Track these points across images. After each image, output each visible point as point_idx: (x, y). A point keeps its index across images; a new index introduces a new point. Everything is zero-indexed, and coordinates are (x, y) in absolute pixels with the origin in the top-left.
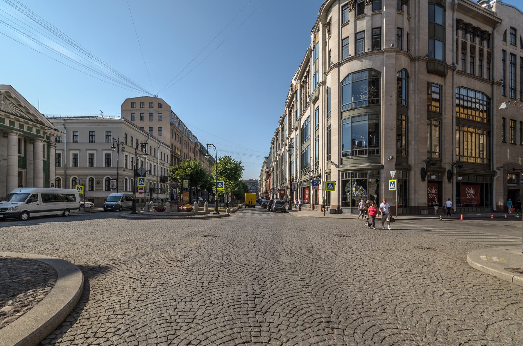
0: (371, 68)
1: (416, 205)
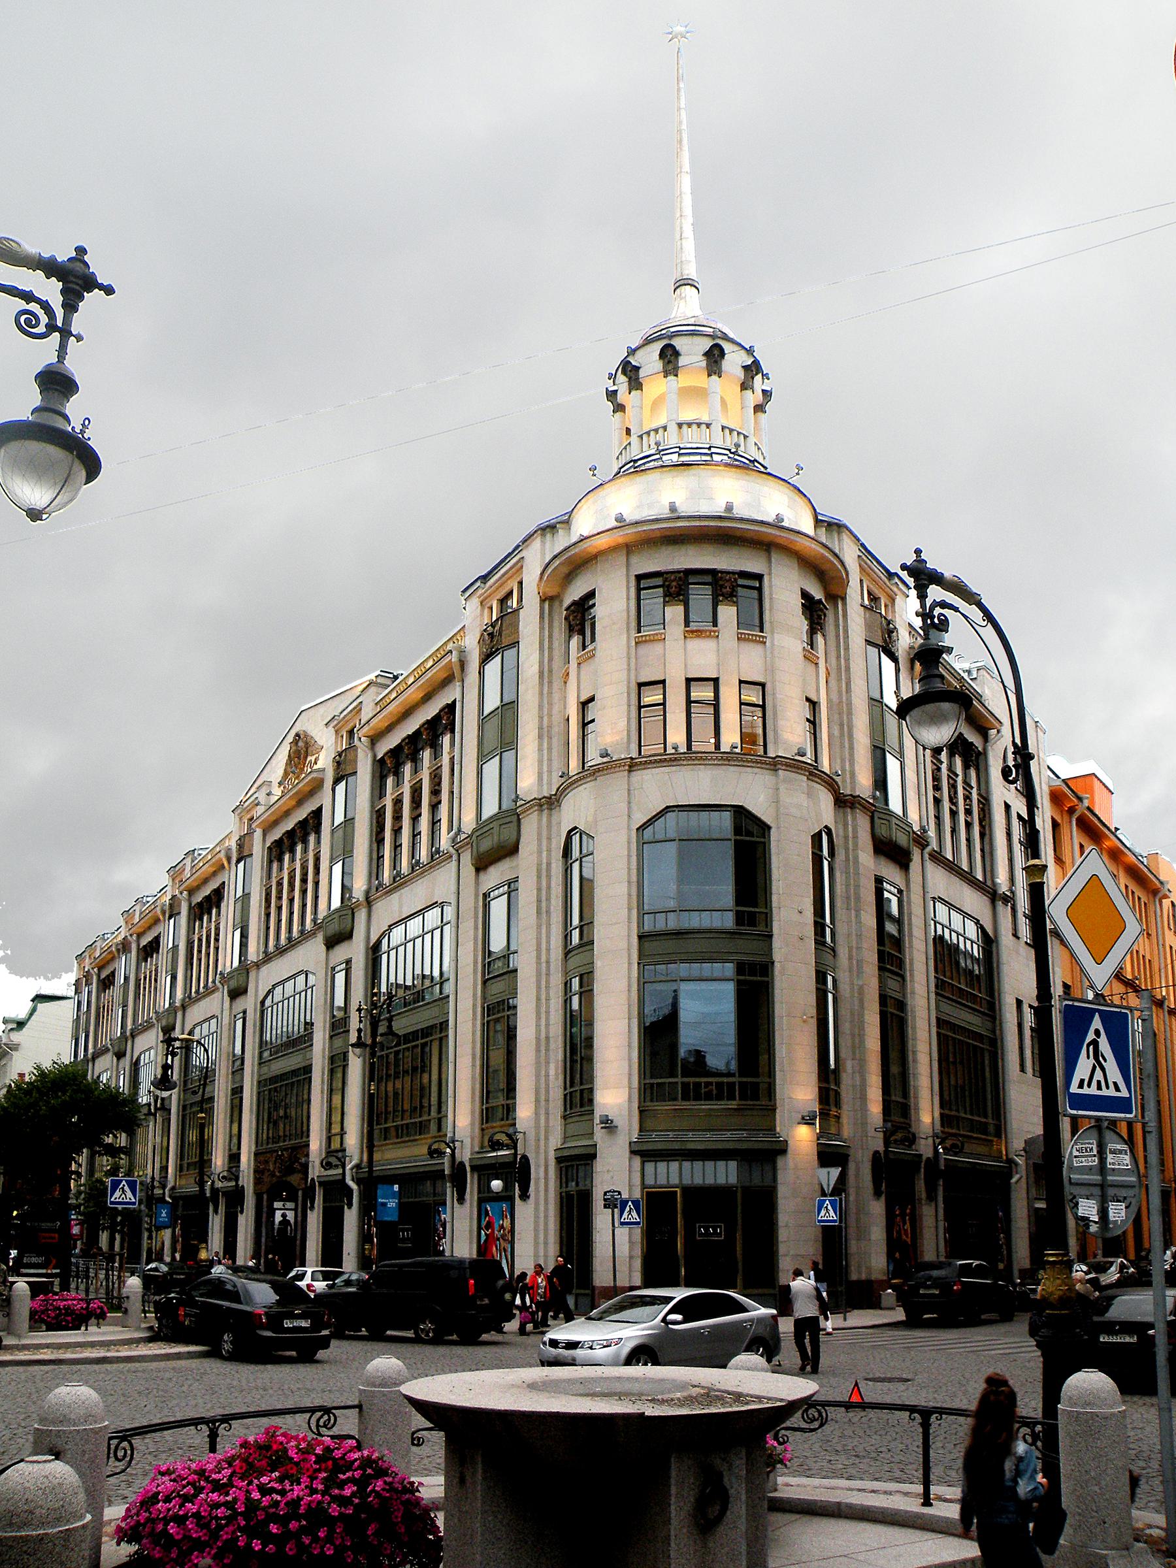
0: (741, 807)
1: (864, 1277)
